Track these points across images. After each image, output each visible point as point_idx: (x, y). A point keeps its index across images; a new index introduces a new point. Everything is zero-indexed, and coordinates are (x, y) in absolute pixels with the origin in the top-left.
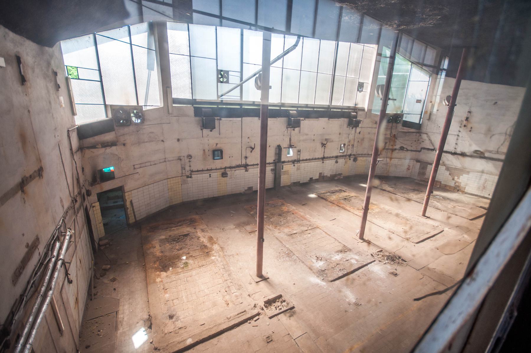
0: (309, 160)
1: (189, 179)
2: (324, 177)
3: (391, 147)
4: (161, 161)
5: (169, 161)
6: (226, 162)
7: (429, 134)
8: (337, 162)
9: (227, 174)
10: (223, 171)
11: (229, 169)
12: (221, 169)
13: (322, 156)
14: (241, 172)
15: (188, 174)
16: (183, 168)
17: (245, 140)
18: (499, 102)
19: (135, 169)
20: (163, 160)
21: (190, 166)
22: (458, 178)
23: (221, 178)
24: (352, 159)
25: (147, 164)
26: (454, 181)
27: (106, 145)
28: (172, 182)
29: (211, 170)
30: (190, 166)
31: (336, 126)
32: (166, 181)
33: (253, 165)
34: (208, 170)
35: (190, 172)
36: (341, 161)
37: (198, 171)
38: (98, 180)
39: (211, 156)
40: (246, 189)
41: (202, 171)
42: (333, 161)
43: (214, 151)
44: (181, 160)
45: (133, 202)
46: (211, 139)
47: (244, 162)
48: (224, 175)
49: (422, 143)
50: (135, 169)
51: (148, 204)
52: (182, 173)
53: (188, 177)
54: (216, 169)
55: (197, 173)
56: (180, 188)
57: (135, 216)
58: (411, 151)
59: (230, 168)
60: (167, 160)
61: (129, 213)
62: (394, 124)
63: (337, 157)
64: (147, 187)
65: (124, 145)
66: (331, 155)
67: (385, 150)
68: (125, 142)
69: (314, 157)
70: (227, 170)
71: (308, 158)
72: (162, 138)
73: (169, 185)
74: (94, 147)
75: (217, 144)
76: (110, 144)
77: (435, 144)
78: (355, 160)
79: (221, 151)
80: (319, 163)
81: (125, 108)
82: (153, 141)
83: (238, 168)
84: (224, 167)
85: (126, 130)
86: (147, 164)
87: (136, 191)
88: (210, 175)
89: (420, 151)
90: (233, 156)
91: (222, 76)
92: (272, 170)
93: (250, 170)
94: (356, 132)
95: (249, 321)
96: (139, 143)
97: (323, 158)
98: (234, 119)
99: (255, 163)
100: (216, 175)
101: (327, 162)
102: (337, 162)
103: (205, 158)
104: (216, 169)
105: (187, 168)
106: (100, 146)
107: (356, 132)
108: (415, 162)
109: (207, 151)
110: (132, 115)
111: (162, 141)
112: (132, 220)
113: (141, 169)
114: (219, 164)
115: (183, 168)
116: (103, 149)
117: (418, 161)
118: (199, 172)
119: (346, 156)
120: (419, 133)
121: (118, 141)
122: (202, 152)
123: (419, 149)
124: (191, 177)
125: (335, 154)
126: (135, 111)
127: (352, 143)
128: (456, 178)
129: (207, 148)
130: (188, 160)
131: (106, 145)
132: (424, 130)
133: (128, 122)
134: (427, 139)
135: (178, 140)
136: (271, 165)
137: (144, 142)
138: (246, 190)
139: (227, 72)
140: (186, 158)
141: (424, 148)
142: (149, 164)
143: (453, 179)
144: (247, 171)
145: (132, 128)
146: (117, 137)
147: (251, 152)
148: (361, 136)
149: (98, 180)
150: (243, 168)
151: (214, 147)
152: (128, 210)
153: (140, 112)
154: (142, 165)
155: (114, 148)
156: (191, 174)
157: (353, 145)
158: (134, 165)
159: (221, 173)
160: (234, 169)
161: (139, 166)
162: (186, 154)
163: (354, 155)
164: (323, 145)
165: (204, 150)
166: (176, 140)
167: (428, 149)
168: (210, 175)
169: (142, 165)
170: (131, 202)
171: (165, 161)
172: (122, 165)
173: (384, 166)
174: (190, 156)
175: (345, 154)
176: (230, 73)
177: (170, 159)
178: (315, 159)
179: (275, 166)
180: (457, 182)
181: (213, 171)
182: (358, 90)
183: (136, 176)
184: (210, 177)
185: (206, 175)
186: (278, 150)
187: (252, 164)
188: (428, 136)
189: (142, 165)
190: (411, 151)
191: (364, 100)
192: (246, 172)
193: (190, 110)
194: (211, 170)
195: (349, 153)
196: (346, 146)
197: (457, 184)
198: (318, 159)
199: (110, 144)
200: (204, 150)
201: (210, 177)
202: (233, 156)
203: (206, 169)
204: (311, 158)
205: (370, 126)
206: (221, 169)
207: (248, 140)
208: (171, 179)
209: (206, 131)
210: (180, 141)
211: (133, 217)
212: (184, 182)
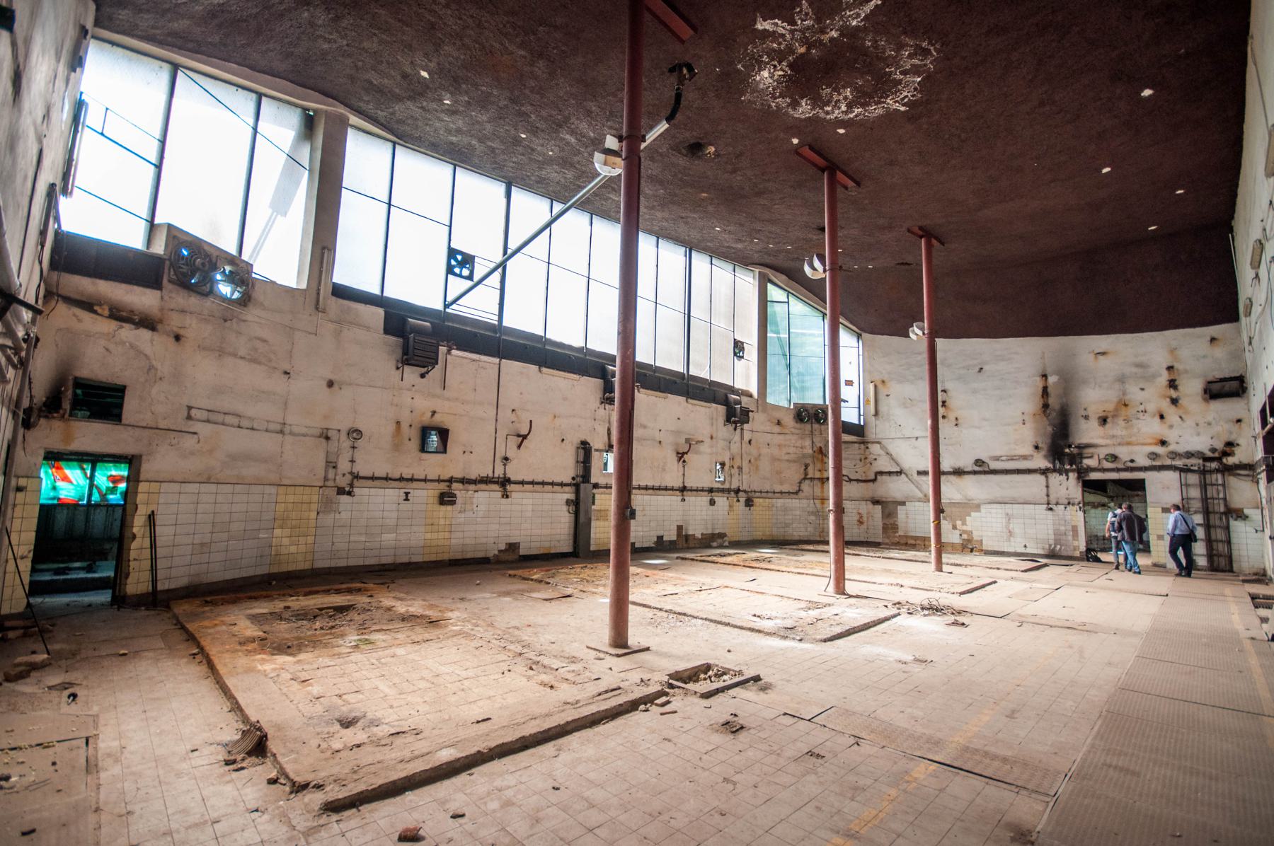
0: (653, 488)
1: (345, 498)
2: (687, 537)
3: (818, 475)
4: (272, 427)
5: (291, 433)
6: (452, 464)
7: (884, 442)
8: (712, 503)
9: (454, 496)
10: (443, 486)
11: (460, 486)
12: (439, 481)
13: (678, 484)
14: (486, 498)
15: (343, 482)
16: (331, 464)
17: (505, 415)
18: (986, 368)
19: (189, 417)
20: (278, 427)
21: (352, 461)
22: (964, 523)
23: (437, 507)
24: (742, 500)
25: (229, 419)
26: (957, 532)
27: (119, 315)
28: (291, 498)
29: (412, 480)
30: (352, 461)
31: (702, 418)
32: (273, 490)
33: (522, 483)
34: (401, 479)
35: (349, 477)
36: (721, 501)
37: (373, 478)
38: (66, 405)
39: (415, 444)
40: (503, 547)
41: (387, 479)
42: (705, 499)
43: (425, 432)
44: (327, 438)
45: (159, 519)
46: (417, 396)
47: (499, 472)
48: (446, 499)
49: (875, 463)
50: (189, 417)
51: (202, 545)
52: (326, 479)
53: (341, 491)
54: (425, 480)
55: (370, 483)
56: (313, 523)
57: (154, 569)
58: (858, 481)
59: (464, 481)
60: (287, 429)
61: (133, 555)
62: (816, 426)
63: (711, 490)
64: (213, 487)
65: (178, 338)
66: (700, 485)
67: (807, 482)
68: (182, 332)
69: (663, 485)
70: (455, 485)
71: (650, 484)
72: (287, 367)
73: (281, 507)
74: (88, 305)
75: (434, 413)
76: (136, 318)
77: (900, 461)
78: (749, 503)
79: (444, 434)
80: (673, 500)
81: (206, 248)
82: (260, 363)
83: (483, 486)
84: (447, 477)
85: (193, 301)
86: (229, 419)
87: (175, 487)
88: (407, 494)
89: (874, 480)
90: (472, 452)
91: (459, 261)
92: (568, 502)
93: (514, 494)
94: (742, 438)
95: (642, 707)
96: (221, 352)
97: (683, 489)
98: (484, 358)
99: (527, 479)
100: (424, 496)
101: (691, 499)
102: (712, 503)
103: (397, 447)
104: (425, 480)
105: (344, 466)
106: (107, 313)
107: (742, 438)
108: (870, 506)
109: (405, 426)
110: (219, 277)
111: (286, 373)
112: (137, 583)
113: (210, 426)
114: (433, 465)
115: (331, 464)
116: (113, 324)
117: (876, 502)
118: (377, 483)
119: (729, 491)
120: (863, 443)
121: (161, 321)
122: (391, 427)
123: (872, 477)
124: (349, 493)
125: (707, 484)
126: (228, 269)
127: (737, 463)
128: (959, 523)
129: (406, 418)
130: (346, 444)
131: (119, 315)
132: (870, 435)
133: (205, 290)
134: (882, 452)
135: (330, 384)
136: (567, 489)
137: (235, 355)
138: (500, 551)
139: (473, 257)
140: (343, 435)
141: (881, 473)
142: (235, 421)
143: (954, 527)
144: (506, 495)
145: (208, 303)
146: (162, 309)
147: (519, 447)
148: (754, 452)
149: (66, 405)
150: (496, 487)
151: (426, 419)
152: (134, 545)
153: (241, 275)
154: (213, 417)
155: (145, 334)
156: (351, 485)
157: (740, 468)
158: (190, 408)
159: (437, 493)
160: (472, 487)
161: (204, 415)
162: (344, 427)
163: (745, 491)
164: (681, 456)
165: (398, 423)
166: (324, 383)
167: (890, 473)
168: (407, 494)
169: (213, 417)
170: (151, 518)
171: (281, 432)
172: (154, 391)
173: (813, 518)
174: (355, 434)
175: (727, 486)
176: (477, 260)
177: (295, 429)
178: (666, 489)
179: (577, 492)
180: (965, 532)
181: (415, 484)
182: (735, 354)
183: (189, 442)
184: (407, 499)
185: (392, 494)
186: (582, 452)
187: (520, 478)
188: (883, 448)
189: (214, 417)
190: (858, 481)
191: (748, 377)
192: (504, 501)
193: (377, 315)
194: (412, 480)
195: (734, 486)
196: (727, 467)
197: (965, 536)
198: (672, 489)
199: (136, 318)
200: (398, 423)
201: (407, 499)
202: (472, 452)
203: (398, 476)
204: (657, 484)
205: (768, 428)
206: (439, 481)
207: (513, 417)
208: (291, 490)
209: (411, 373)
210: (336, 387)
211: (146, 575)
212: (327, 506)
